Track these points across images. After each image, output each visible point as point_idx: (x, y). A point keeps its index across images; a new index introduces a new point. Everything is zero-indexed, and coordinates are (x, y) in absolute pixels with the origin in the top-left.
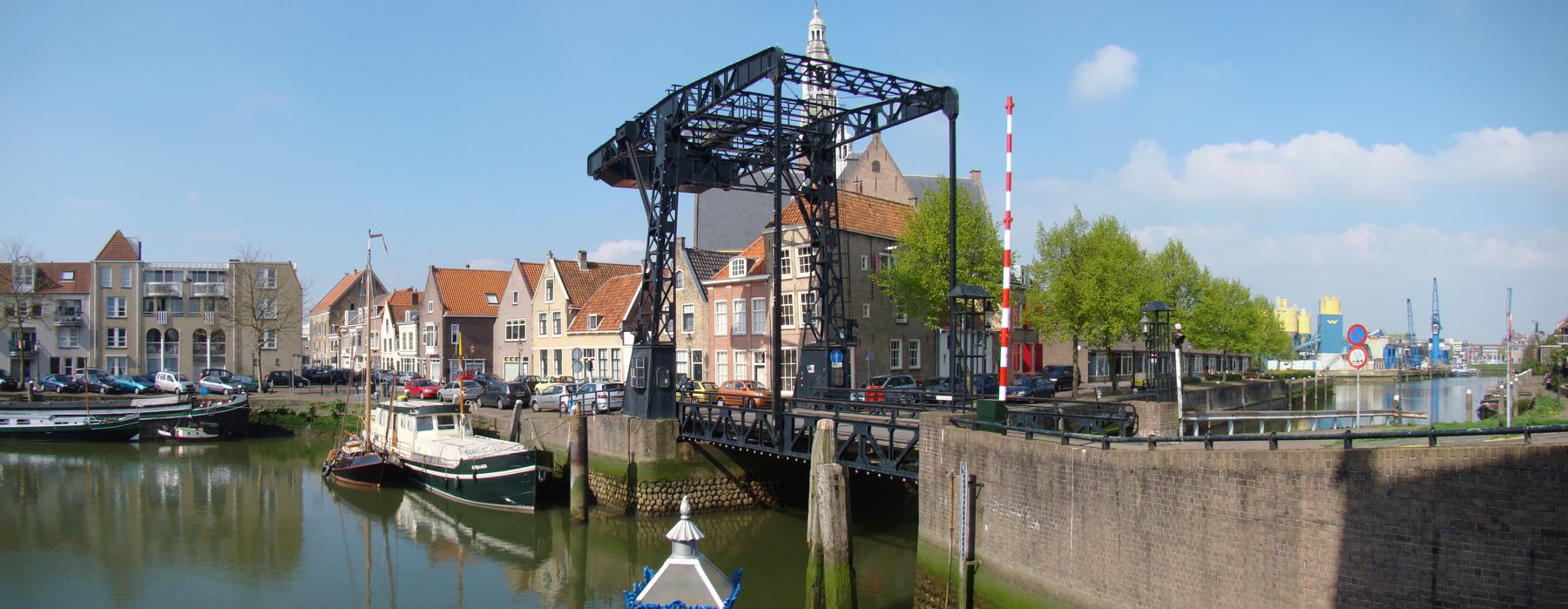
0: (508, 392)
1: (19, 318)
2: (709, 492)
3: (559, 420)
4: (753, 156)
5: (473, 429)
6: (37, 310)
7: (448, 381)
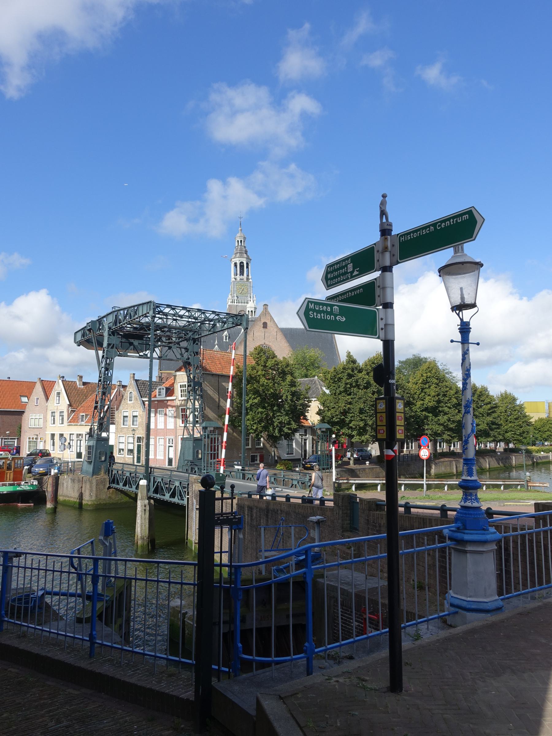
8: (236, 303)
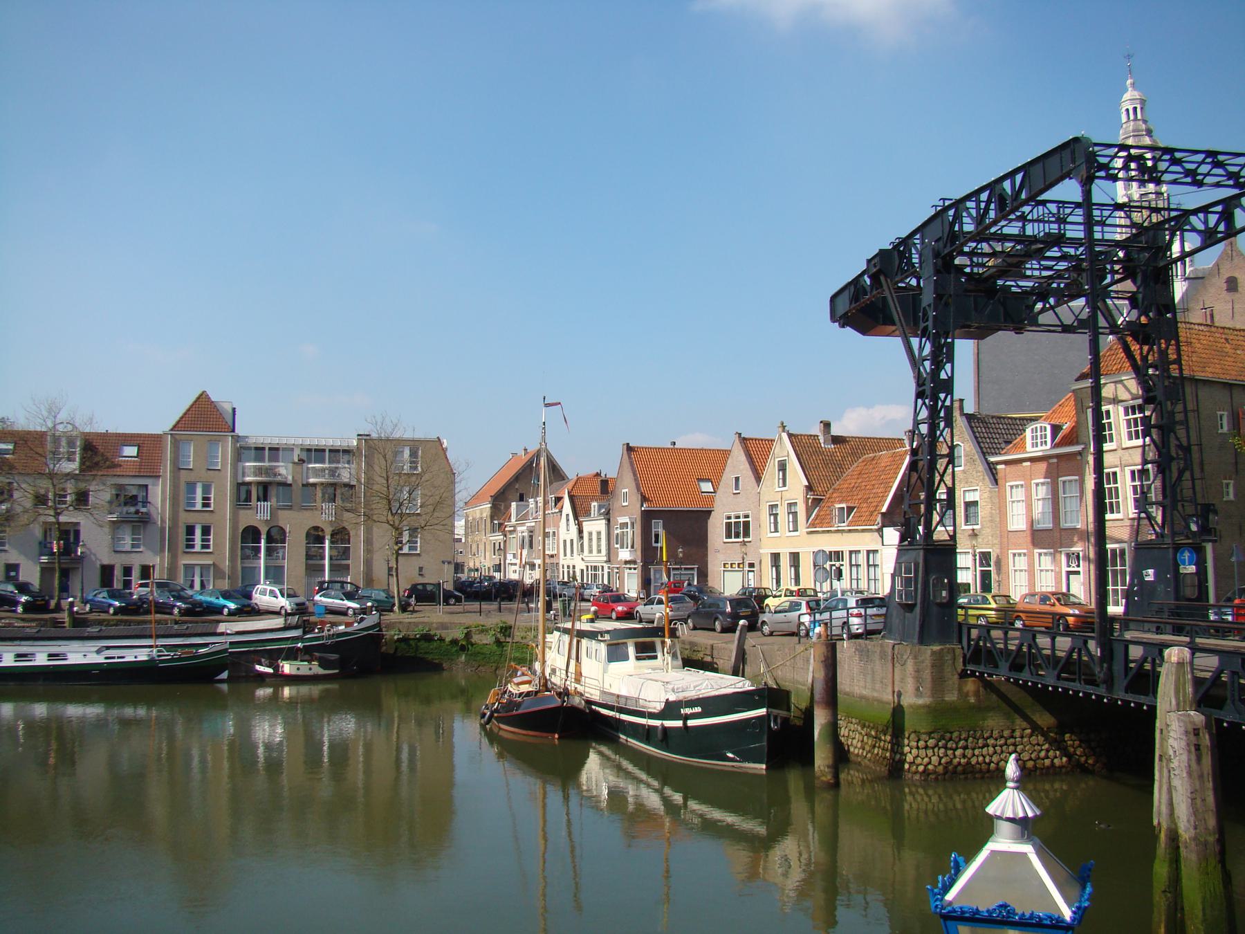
0: (729, 609)
1: (56, 509)
2: (1004, 748)
3: (797, 646)
4: (1054, 285)
5: (683, 659)
6: (82, 499)
7: (648, 595)
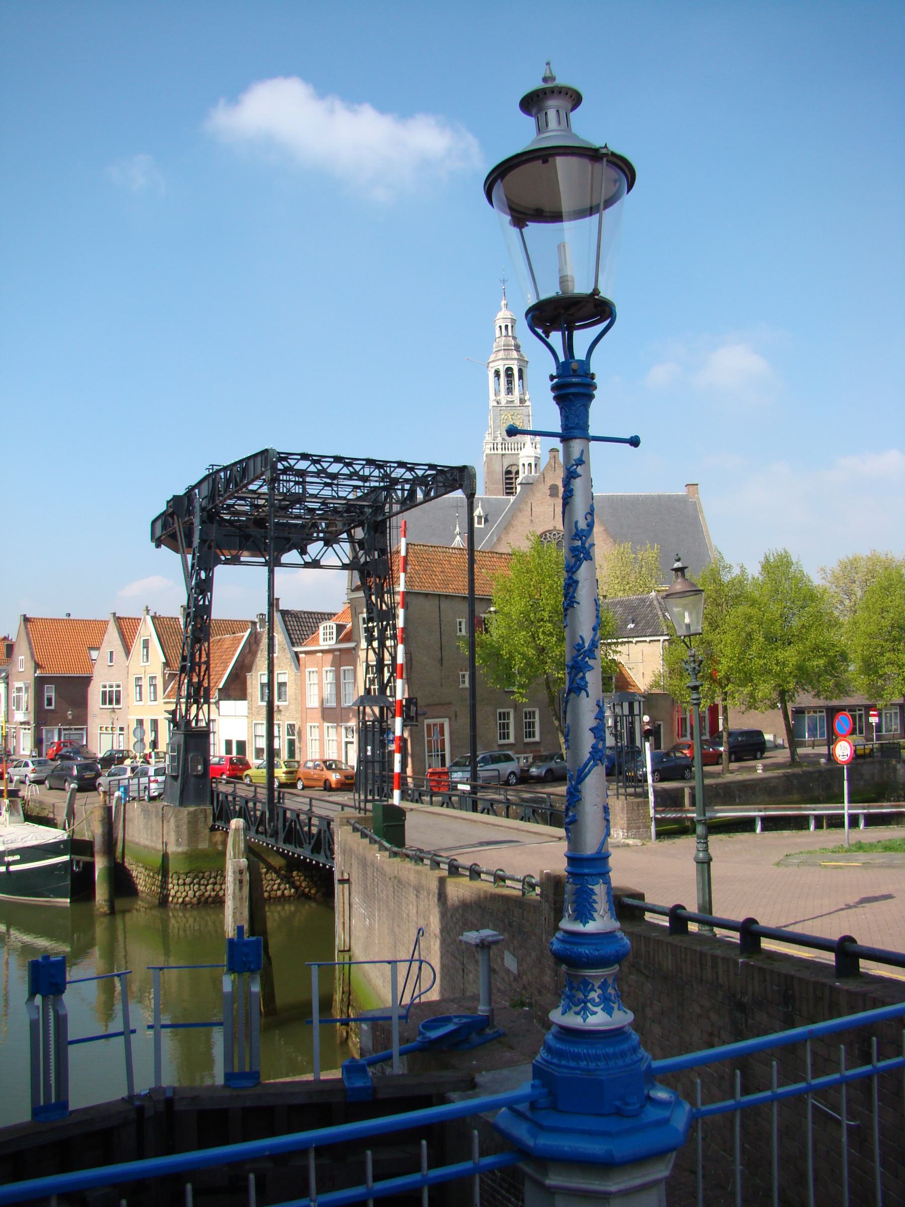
0: (75, 772)
8: (500, 450)
